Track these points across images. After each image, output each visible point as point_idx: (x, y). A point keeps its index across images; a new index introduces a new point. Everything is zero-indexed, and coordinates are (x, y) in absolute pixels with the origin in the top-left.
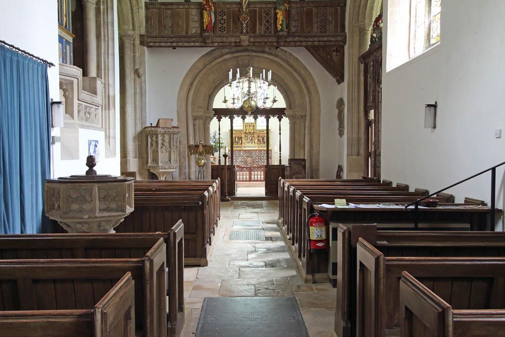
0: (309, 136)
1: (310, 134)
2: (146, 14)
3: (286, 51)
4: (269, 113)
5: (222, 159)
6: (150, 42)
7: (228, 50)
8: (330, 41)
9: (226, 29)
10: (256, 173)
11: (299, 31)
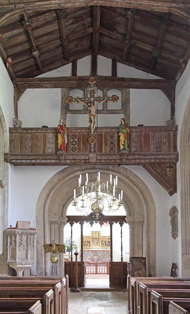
0: (147, 238)
1: (148, 237)
2: (11, 137)
3: (126, 169)
4: (112, 220)
5: (74, 256)
6: (13, 159)
7: (79, 168)
8: (164, 159)
9: (77, 149)
10: (101, 267)
11: (138, 151)
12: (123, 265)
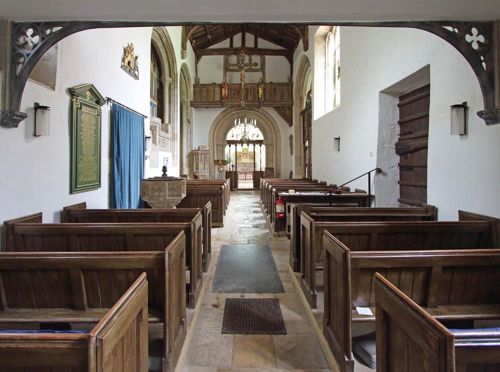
1: (276, 154)
3: (263, 110)
5: (231, 167)
12: (261, 173)
